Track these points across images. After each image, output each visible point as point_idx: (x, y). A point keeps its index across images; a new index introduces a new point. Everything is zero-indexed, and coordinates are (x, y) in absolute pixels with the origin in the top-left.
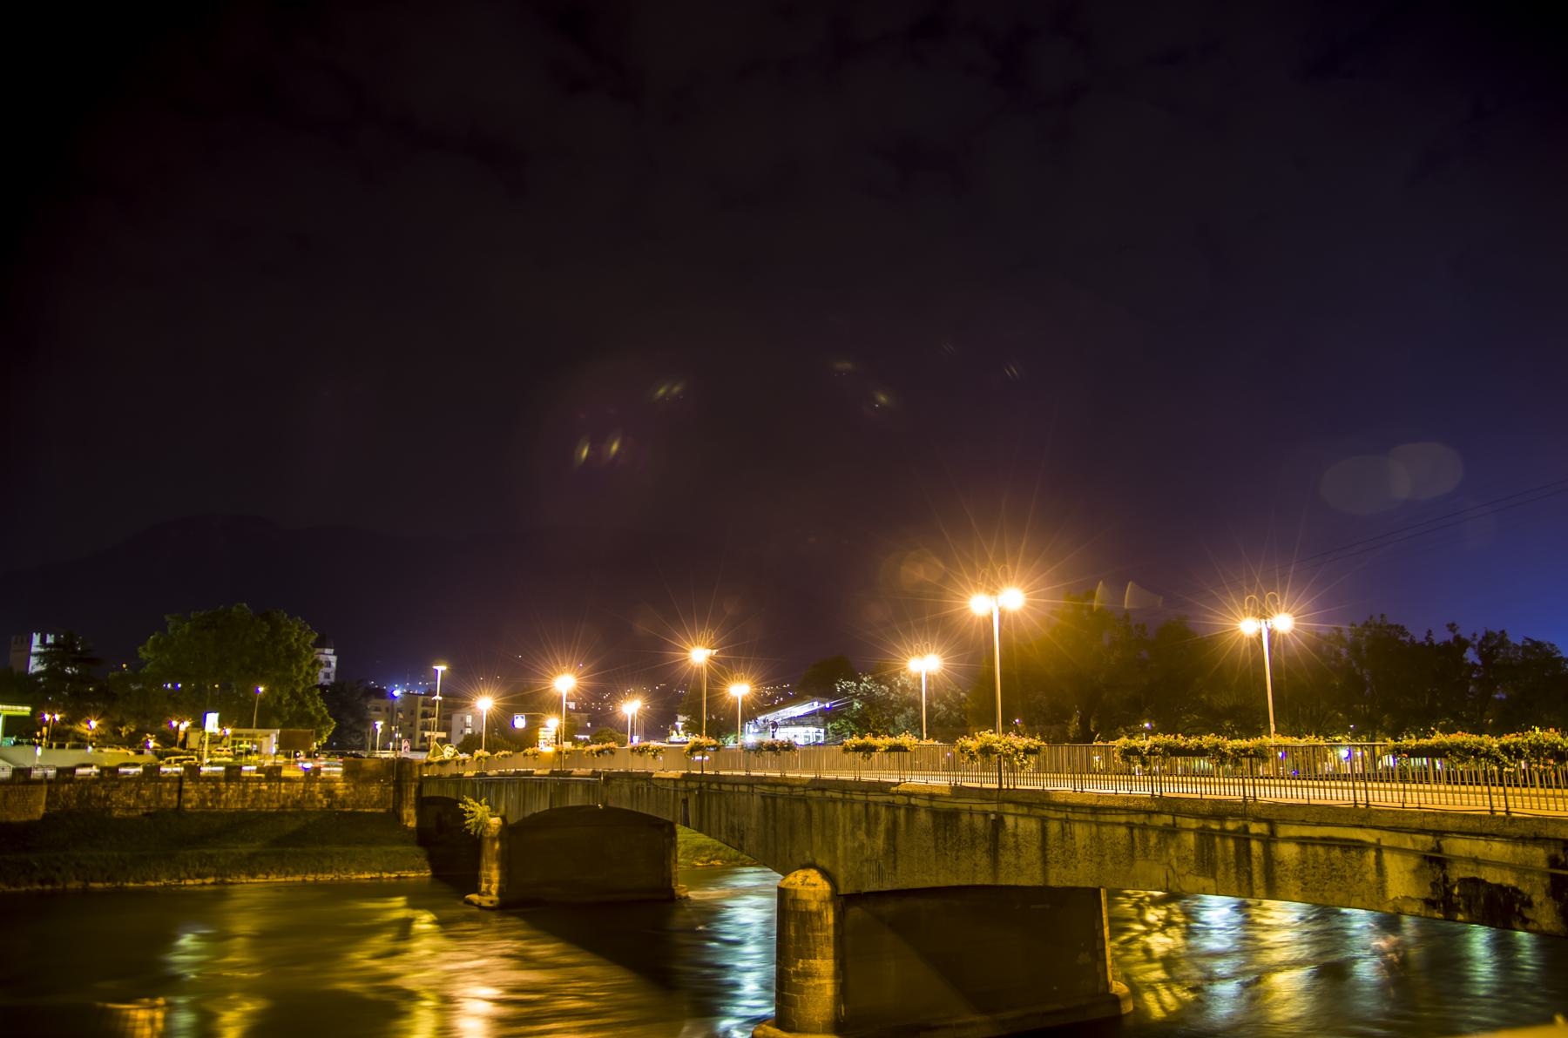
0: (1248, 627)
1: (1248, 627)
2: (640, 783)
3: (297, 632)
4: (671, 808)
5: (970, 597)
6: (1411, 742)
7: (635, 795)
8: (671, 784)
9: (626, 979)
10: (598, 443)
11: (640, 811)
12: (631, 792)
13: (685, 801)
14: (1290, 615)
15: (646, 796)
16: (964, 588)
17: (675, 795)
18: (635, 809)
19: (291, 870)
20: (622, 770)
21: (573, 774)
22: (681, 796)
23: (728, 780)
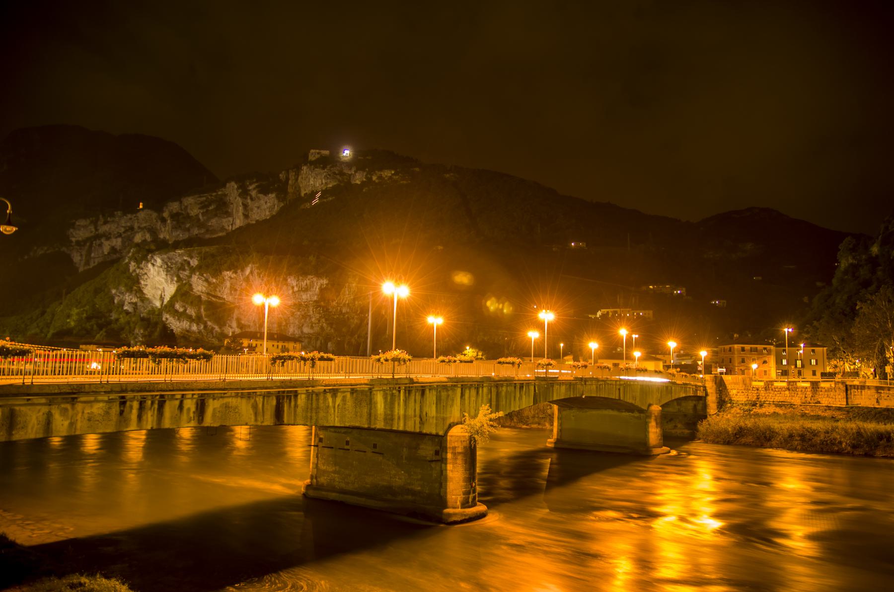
0: (258, 299)
1: (258, 299)
2: (601, 383)
3: (533, 305)
4: (614, 393)
5: (408, 298)
6: (30, 345)
7: (598, 389)
8: (614, 383)
9: (488, 523)
10: (677, 293)
11: (601, 396)
12: (597, 387)
13: (619, 389)
14: (255, 295)
15: (604, 389)
16: (614, 323)
17: (616, 387)
18: (598, 396)
19: (555, 467)
20: (595, 377)
21: (558, 379)
22: (618, 387)
23: (87, 389)
